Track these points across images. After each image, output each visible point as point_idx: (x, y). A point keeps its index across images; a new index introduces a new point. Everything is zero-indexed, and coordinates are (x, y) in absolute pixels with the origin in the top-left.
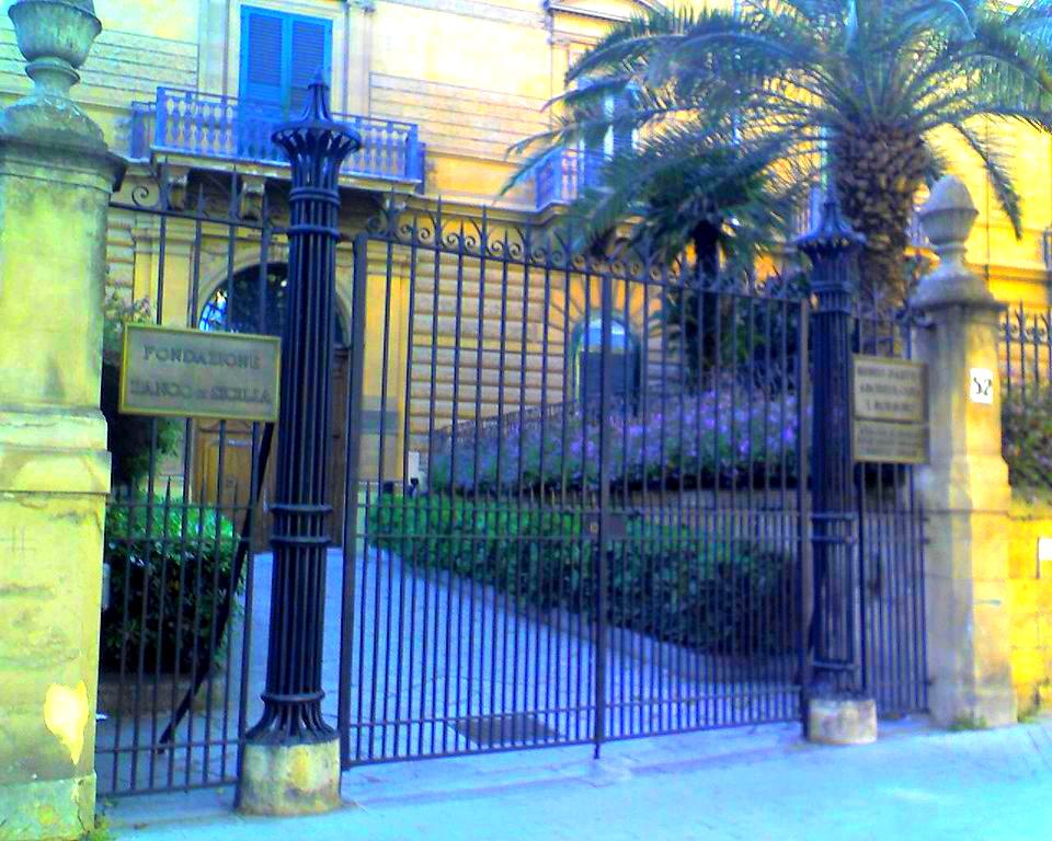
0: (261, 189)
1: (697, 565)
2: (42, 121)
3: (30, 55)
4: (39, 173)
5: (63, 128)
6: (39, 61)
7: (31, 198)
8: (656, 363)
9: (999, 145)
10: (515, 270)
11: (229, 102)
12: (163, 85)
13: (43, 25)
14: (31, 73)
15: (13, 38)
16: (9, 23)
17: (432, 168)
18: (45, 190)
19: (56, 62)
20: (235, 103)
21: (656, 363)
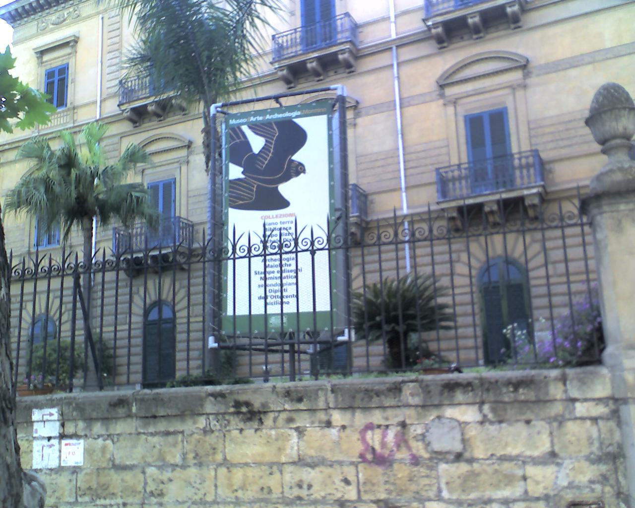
0: (495, 208)
1: (327, 409)
2: (618, 177)
3: (603, 142)
4: (622, 207)
5: (631, 177)
6: (608, 144)
7: (620, 222)
8: (465, 315)
9: (19, 212)
10: (439, 245)
11: (463, 166)
12: (437, 166)
13: (608, 124)
14: (604, 152)
15: (591, 137)
16: (587, 130)
17: (550, 171)
18: (627, 215)
19: (618, 141)
20: (466, 166)
21: (465, 315)
